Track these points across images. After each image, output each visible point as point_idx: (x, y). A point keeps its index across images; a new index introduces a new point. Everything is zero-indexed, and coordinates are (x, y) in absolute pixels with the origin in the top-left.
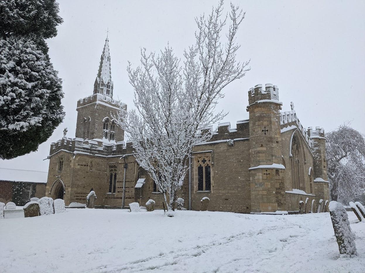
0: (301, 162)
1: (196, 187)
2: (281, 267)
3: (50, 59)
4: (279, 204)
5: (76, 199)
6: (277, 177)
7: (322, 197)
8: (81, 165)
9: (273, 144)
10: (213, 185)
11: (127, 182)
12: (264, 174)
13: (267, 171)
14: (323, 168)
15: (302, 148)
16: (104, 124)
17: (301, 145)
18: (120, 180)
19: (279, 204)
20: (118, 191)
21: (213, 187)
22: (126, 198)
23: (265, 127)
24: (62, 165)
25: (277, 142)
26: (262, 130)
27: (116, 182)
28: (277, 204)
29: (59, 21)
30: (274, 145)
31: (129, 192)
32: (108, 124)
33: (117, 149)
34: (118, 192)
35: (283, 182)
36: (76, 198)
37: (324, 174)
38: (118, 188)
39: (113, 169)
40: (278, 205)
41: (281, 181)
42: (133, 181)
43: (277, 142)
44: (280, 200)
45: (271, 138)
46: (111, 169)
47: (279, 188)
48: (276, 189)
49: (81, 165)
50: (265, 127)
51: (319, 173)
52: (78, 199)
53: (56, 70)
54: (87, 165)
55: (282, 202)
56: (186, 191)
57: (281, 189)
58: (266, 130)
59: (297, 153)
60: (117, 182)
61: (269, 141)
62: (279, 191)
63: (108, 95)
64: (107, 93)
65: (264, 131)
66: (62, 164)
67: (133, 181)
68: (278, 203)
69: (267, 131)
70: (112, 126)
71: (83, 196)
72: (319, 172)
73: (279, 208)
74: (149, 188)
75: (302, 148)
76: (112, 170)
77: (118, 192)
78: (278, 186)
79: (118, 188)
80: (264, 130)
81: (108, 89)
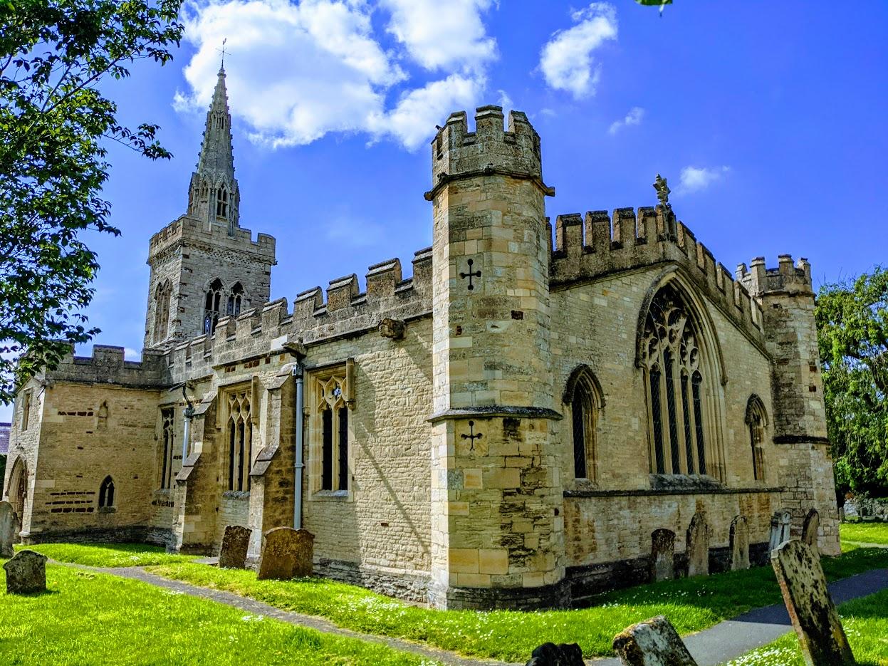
0: (707, 379)
1: (315, 477)
4: (514, 553)
5: (54, 511)
6: (512, 447)
7: (805, 492)
8: (70, 414)
9: (498, 323)
12: (464, 436)
13: (471, 424)
14: (806, 393)
15: (707, 329)
16: (209, 297)
17: (704, 320)
18: (178, 454)
19: (514, 553)
23: (470, 262)
25: (517, 315)
26: (459, 272)
28: (505, 554)
29: (189, 65)
30: (505, 325)
32: (221, 293)
35: (536, 464)
36: (52, 506)
37: (813, 414)
40: (511, 556)
41: (526, 463)
43: (517, 315)
44: (523, 538)
45: (490, 301)
47: (519, 491)
48: (505, 494)
49: (70, 414)
50: (470, 262)
51: (793, 411)
52: (59, 510)
54: (88, 411)
55: (531, 543)
56: (286, 492)
57: (530, 493)
58: (475, 270)
59: (690, 348)
61: (482, 315)
62: (518, 500)
63: (221, 216)
64: (218, 214)
65: (467, 278)
68: (511, 550)
69: (479, 274)
70: (231, 299)
71: (77, 502)
72: (792, 408)
73: (517, 570)
74: (218, 480)
75: (707, 329)
78: (513, 481)
80: (468, 272)
81: (222, 201)
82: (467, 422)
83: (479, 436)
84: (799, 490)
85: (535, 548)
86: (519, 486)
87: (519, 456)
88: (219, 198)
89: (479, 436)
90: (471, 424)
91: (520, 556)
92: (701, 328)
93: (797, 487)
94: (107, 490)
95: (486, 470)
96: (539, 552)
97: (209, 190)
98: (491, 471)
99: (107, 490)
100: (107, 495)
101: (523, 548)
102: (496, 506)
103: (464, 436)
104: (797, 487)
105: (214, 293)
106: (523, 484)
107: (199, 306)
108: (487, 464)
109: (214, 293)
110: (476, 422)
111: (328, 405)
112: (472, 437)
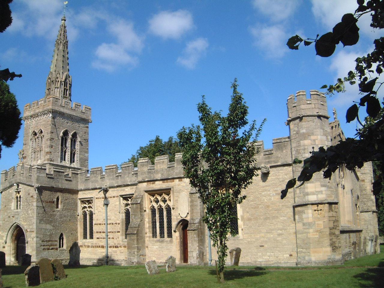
2: (80, 106)
3: (5, 31)
10: (242, 227)
11: (110, 224)
12: (315, 210)
20: (98, 237)
21: (242, 230)
22: (111, 247)
24: (20, 201)
27: (93, 224)
31: (113, 238)
33: (223, 206)
34: (98, 238)
36: (43, 247)
38: (97, 232)
39: (87, 206)
42: (119, 224)
46: (83, 206)
53: (228, 247)
55: (337, 245)
57: (336, 229)
60: (95, 224)
66: (19, 200)
67: (119, 224)
76: (85, 207)
77: (98, 238)
79: (97, 232)
82: (316, 205)
83: (321, 210)
84: (368, 229)
85: (338, 246)
86: (333, 227)
87: (332, 217)
88: (64, 86)
89: (321, 210)
90: (318, 206)
91: (335, 249)
92: (346, 174)
93: (367, 228)
94: (61, 240)
95: (324, 222)
96: (338, 247)
97: (60, 82)
98: (326, 222)
99: (61, 240)
100: (61, 243)
101: (335, 247)
102: (328, 233)
103: (315, 210)
104: (367, 228)
105: (64, 138)
106: (334, 226)
107: (59, 145)
108: (324, 220)
109: (64, 138)
110: (319, 205)
111: (157, 199)
112: (318, 211)
